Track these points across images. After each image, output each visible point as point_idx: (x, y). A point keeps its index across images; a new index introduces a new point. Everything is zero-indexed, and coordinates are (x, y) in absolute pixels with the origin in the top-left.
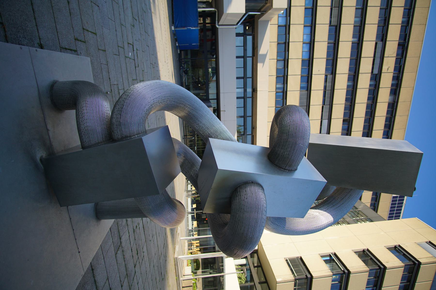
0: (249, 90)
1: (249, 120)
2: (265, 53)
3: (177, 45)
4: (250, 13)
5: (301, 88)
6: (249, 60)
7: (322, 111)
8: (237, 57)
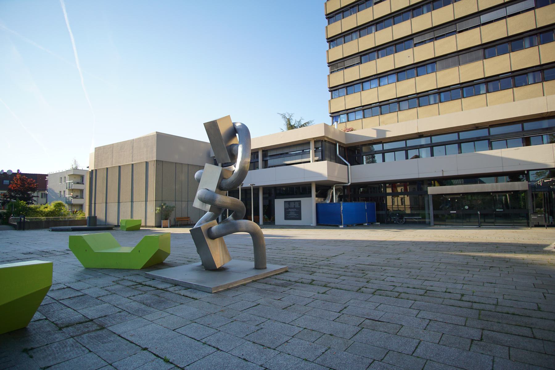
0: (423, 141)
1: (463, 136)
2: (375, 131)
3: (342, 226)
4: (338, 153)
5: (433, 71)
6: (387, 146)
7: (467, 30)
8: (432, 155)
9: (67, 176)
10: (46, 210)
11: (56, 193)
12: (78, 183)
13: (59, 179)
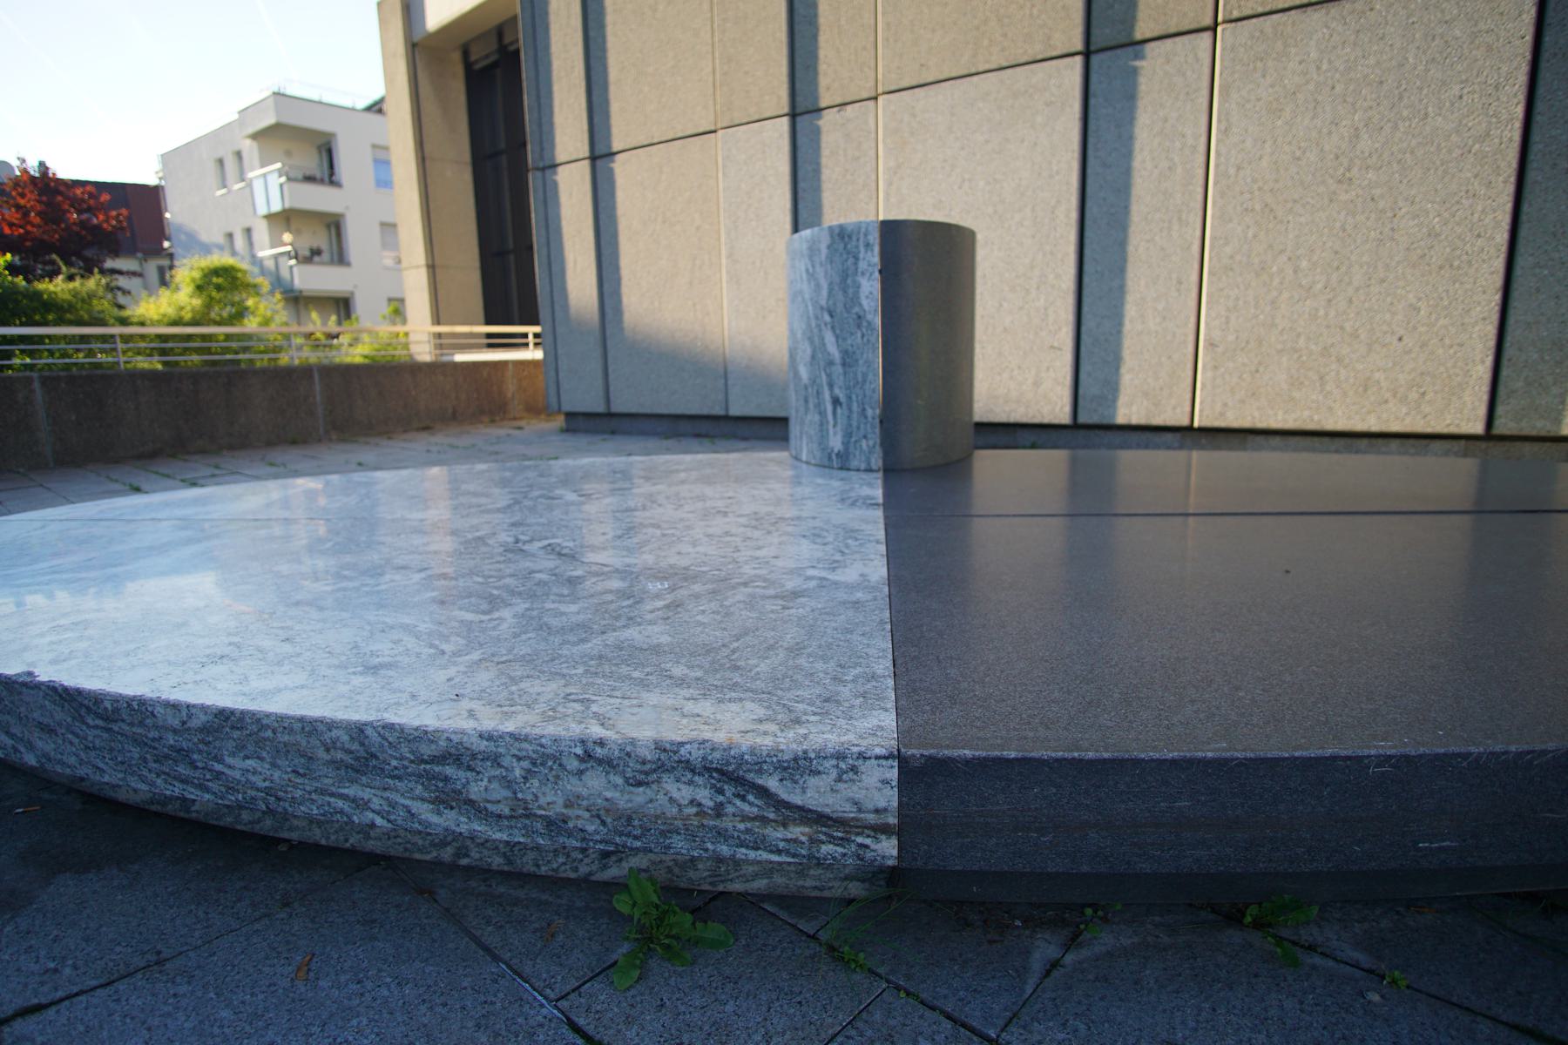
9: (248, 146)
12: (309, 179)
13: (211, 167)
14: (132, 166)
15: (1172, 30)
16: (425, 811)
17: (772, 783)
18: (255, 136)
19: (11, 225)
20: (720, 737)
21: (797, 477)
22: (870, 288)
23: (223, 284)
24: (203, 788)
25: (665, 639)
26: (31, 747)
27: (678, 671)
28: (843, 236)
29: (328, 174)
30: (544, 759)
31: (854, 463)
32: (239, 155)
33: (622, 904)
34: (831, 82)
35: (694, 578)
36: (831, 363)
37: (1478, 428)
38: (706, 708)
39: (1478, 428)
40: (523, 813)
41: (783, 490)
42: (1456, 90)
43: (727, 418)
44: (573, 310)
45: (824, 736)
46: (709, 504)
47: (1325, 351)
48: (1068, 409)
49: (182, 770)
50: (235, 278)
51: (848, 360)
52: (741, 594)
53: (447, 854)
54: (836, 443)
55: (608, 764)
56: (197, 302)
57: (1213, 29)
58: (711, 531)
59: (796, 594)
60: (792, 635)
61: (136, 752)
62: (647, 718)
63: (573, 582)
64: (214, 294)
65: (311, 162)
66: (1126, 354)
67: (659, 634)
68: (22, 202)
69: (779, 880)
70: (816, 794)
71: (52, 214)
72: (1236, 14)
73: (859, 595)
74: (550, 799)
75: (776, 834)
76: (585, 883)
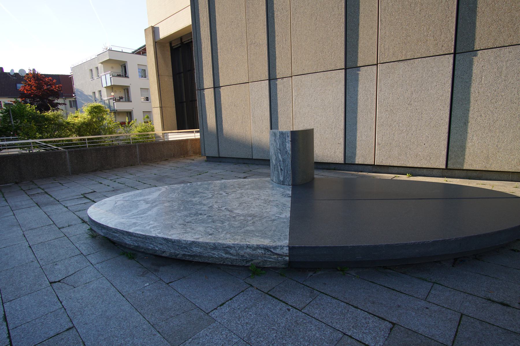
9: (100, 66)
10: (77, 121)
11: (86, 96)
12: (119, 76)
13: (88, 72)
14: (61, 69)
15: (367, 64)
16: (224, 255)
17: (272, 250)
18: (102, 63)
19: (27, 90)
20: (265, 244)
21: (273, 187)
22: (289, 146)
23: (97, 111)
24: (188, 252)
25: (254, 229)
26: (157, 247)
27: (257, 234)
28: (282, 133)
29: (125, 75)
30: (241, 247)
31: (286, 184)
32: (97, 68)
33: (250, 268)
34: (281, 70)
35: (255, 216)
36: (280, 161)
37: (444, 167)
38: (262, 240)
39: (444, 167)
40: (238, 254)
41: (270, 191)
42: (435, 84)
43: (252, 159)
44: (209, 129)
45: (279, 244)
46: (255, 196)
47: (407, 147)
48: (343, 159)
49: (185, 250)
50: (100, 109)
51: (284, 161)
52: (264, 220)
53: (222, 263)
54: (281, 179)
55: (250, 248)
56: (89, 117)
57: (377, 65)
58: (257, 204)
59: (274, 220)
60: (274, 228)
61: (177, 247)
62: (255, 241)
63: (234, 217)
64: (94, 114)
65: (119, 71)
66: (357, 145)
67: (252, 228)
68: (30, 83)
69: (273, 265)
70: (278, 251)
71: (39, 87)
72: (382, 62)
73: (285, 220)
74: (242, 253)
75: (273, 257)
76: (243, 266)
